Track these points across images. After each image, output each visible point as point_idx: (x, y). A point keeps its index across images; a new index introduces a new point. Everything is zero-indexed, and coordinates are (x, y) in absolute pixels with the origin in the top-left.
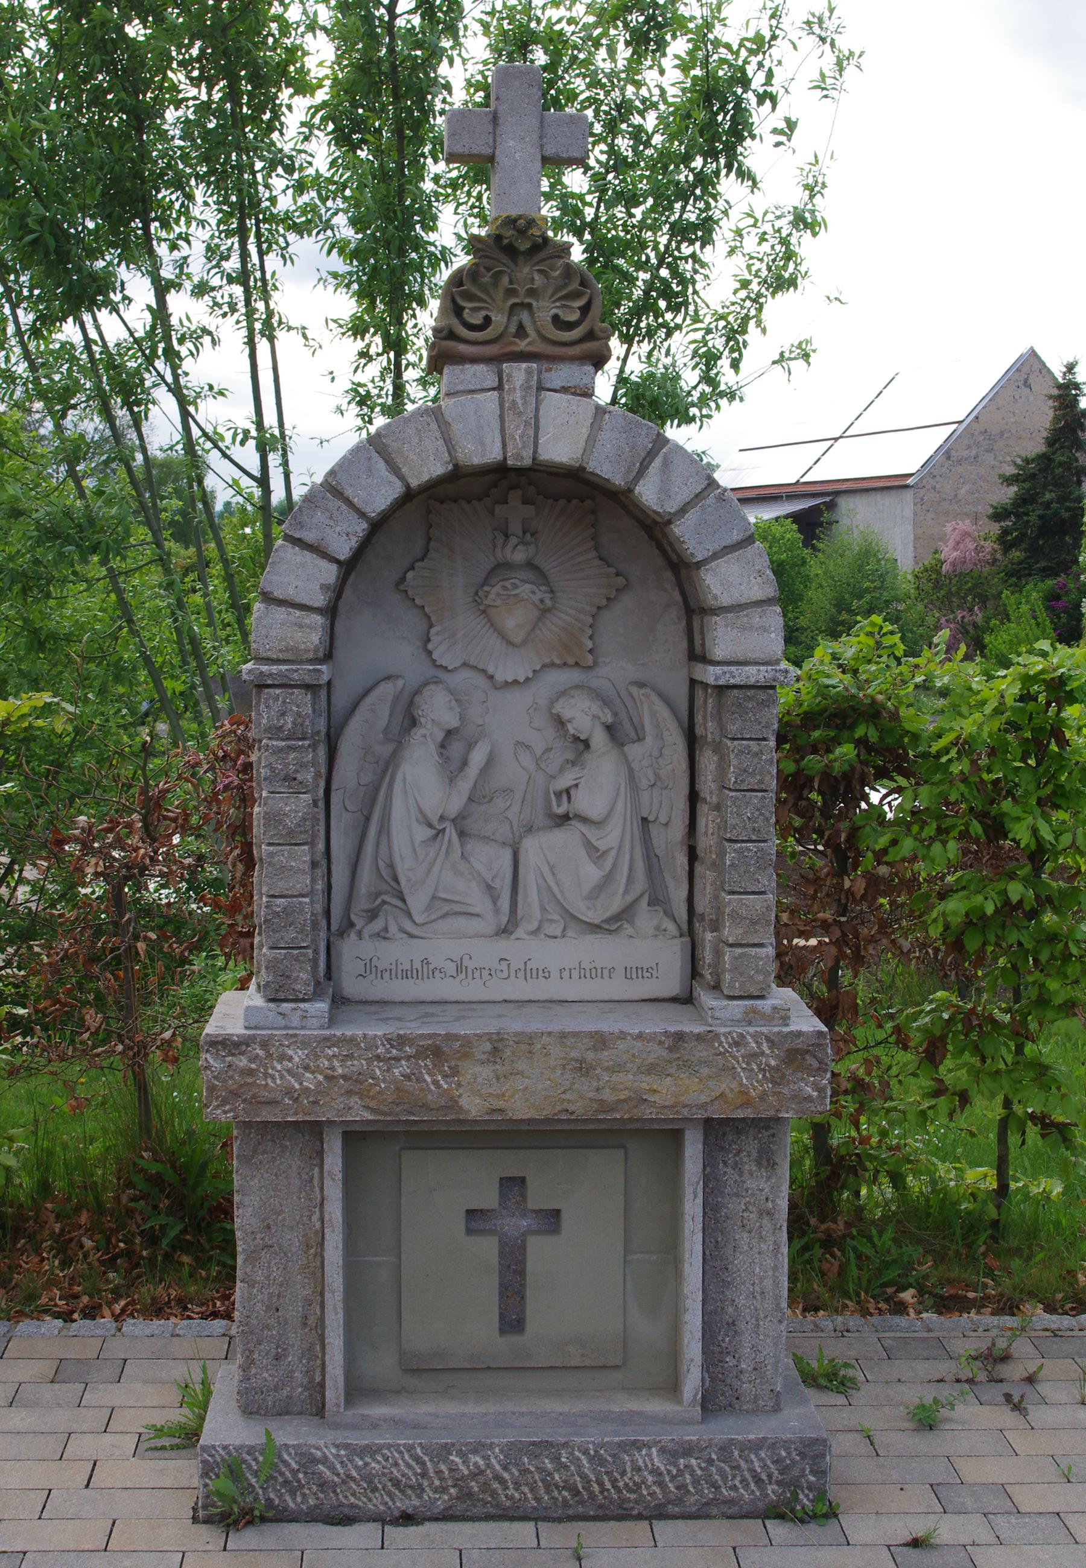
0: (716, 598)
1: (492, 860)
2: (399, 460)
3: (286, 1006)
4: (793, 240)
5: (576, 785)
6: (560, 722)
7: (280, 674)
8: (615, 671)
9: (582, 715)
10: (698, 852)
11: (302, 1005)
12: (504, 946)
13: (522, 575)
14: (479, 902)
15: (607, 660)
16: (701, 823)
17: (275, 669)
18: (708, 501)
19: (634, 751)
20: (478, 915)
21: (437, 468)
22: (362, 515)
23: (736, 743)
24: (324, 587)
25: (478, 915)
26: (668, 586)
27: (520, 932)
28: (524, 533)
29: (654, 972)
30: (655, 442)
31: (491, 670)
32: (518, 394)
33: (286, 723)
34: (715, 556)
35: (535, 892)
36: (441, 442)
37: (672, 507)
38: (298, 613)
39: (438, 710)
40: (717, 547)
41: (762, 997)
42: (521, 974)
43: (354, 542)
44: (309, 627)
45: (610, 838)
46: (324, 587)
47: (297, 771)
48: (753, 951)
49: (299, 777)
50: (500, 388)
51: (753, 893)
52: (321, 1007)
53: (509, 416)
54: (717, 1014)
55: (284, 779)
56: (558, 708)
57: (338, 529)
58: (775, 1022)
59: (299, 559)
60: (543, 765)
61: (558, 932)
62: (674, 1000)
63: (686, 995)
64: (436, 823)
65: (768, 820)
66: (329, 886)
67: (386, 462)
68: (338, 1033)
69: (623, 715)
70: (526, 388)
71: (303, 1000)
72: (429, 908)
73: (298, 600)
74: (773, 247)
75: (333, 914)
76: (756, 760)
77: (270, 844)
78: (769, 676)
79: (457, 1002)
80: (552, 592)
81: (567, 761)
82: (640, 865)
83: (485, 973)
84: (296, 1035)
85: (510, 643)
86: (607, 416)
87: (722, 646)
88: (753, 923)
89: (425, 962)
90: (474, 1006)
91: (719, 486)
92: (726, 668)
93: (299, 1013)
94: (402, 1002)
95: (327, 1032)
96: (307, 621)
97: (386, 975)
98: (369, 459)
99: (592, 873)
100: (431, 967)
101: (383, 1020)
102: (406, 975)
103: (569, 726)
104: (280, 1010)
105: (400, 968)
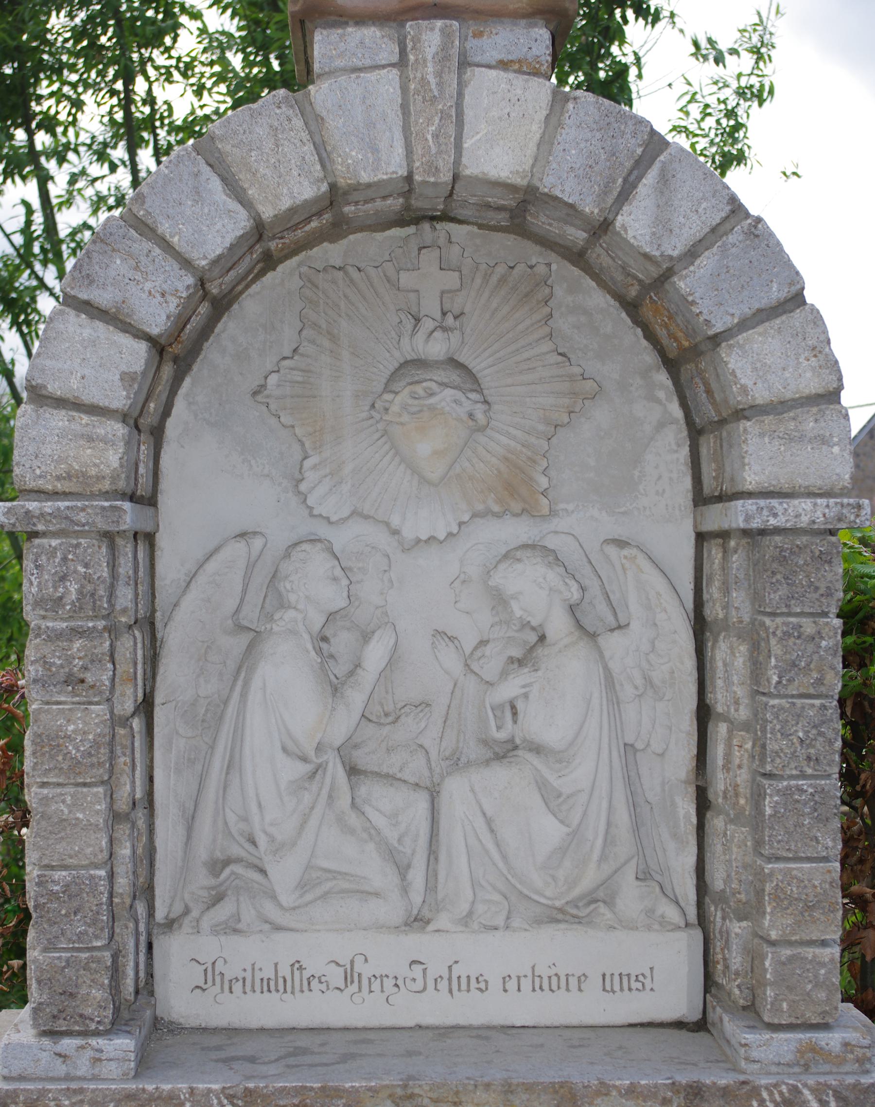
0: (744, 390)
1: (396, 810)
2: (244, 178)
3: (68, 1044)
4: (740, 111)
5: (526, 696)
6: (500, 600)
7: (57, 514)
8: (579, 526)
9: (535, 591)
10: (711, 796)
11: (93, 1042)
12: (415, 943)
13: (441, 375)
14: (376, 872)
15: (570, 507)
16: (718, 752)
17: (48, 506)
18: (731, 238)
19: (613, 643)
20: (377, 894)
21: (306, 189)
22: (186, 263)
23: (779, 620)
24: (127, 378)
25: (377, 894)
26: (661, 395)
27: (443, 921)
28: (444, 314)
29: (648, 982)
30: (647, 145)
31: (395, 521)
32: (430, 69)
33: (67, 592)
34: (744, 325)
35: (464, 859)
36: (309, 148)
37: (675, 247)
38: (85, 419)
39: (314, 587)
40: (746, 309)
41: (825, 1027)
42: (443, 985)
43: (172, 306)
44: (104, 440)
45: (580, 775)
46: (127, 378)
47: (85, 668)
48: (810, 952)
49: (90, 678)
50: (402, 63)
51: (809, 859)
52: (123, 1045)
53: (416, 104)
54: (755, 1054)
55: (66, 682)
56: (497, 579)
57: (148, 286)
58: (847, 1068)
59: (87, 332)
60: (475, 667)
61: (500, 921)
62: (679, 1025)
63: (696, 1016)
64: (312, 754)
65: (831, 743)
66: (151, 851)
67: (223, 179)
68: (150, 1087)
69: (594, 589)
70: (443, 58)
71: (97, 1033)
72: (303, 886)
73: (87, 398)
74: (718, 122)
75: (158, 892)
76: (811, 647)
77: (44, 785)
78: (831, 514)
79: (346, 1029)
80: (486, 402)
81: (511, 660)
82: (623, 817)
83: (389, 983)
84: (81, 1091)
85: (423, 480)
86: (570, 105)
87: (756, 468)
88: (810, 908)
89: (297, 966)
90: (371, 1036)
91: (747, 215)
92: (762, 502)
93: (89, 1053)
94: (262, 1030)
95: (132, 1086)
96: (101, 431)
97: (238, 987)
98: (197, 175)
99: (550, 830)
100: (306, 974)
101: (226, 1061)
102: (267, 986)
103: (515, 605)
104: (58, 1048)
105: (258, 975)
